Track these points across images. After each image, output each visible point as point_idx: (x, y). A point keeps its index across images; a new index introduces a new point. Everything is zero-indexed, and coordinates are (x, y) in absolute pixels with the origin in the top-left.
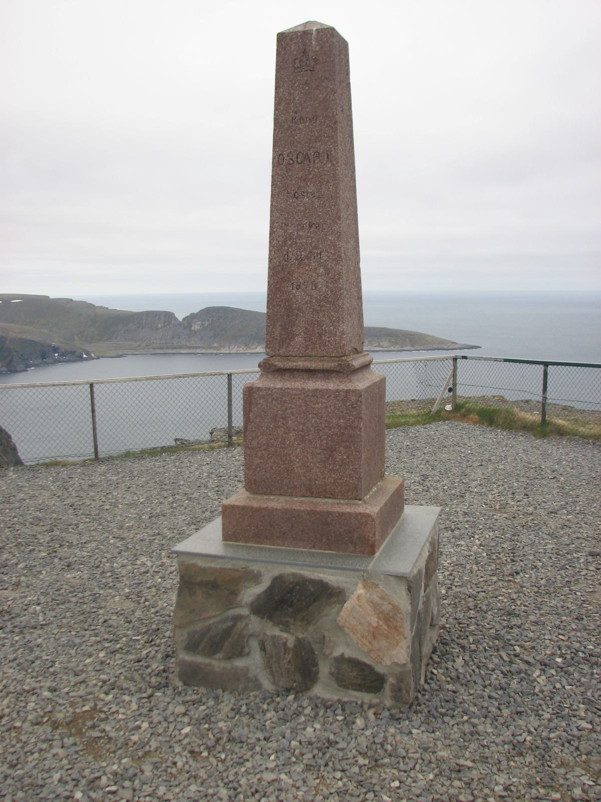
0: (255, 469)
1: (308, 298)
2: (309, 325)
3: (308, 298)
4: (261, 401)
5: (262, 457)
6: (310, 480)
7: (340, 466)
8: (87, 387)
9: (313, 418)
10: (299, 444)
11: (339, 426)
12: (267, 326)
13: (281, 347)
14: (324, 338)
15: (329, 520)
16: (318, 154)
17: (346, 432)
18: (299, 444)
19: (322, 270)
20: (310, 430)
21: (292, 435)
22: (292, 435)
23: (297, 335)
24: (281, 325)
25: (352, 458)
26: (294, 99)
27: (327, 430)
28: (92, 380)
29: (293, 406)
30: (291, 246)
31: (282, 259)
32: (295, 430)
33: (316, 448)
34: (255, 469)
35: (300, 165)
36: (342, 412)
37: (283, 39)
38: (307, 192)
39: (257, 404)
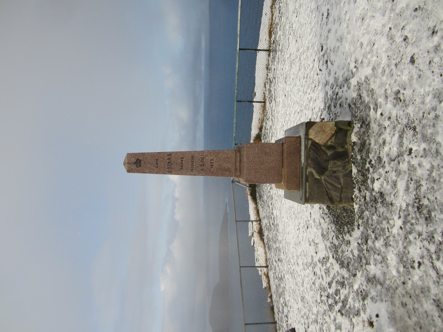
0: (274, 180)
1: (216, 162)
2: (225, 162)
3: (216, 162)
4: (251, 177)
5: (270, 177)
6: (276, 160)
7: (271, 150)
8: (247, 326)
9: (256, 159)
10: (265, 164)
11: (258, 150)
12: (225, 176)
13: (232, 172)
14: (229, 157)
15: (289, 152)
16: (169, 159)
17: (260, 148)
18: (265, 164)
19: (207, 158)
20: (260, 160)
21: (262, 166)
22: (262, 166)
23: (228, 166)
24: (225, 172)
25: (268, 146)
26: (150, 167)
27: (259, 154)
28: (243, 325)
29: (252, 166)
30: (198, 168)
31: (203, 171)
32: (260, 165)
33: (266, 158)
34: (274, 180)
35: (172, 165)
36: (253, 149)
37: (129, 171)
38: (181, 162)
39: (252, 179)
